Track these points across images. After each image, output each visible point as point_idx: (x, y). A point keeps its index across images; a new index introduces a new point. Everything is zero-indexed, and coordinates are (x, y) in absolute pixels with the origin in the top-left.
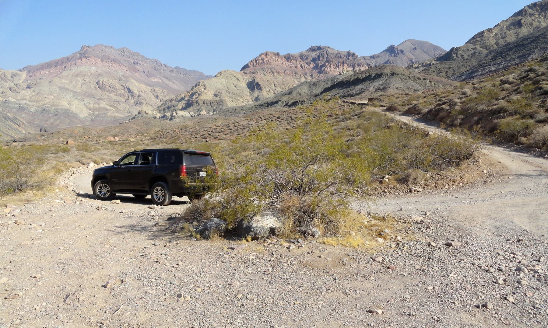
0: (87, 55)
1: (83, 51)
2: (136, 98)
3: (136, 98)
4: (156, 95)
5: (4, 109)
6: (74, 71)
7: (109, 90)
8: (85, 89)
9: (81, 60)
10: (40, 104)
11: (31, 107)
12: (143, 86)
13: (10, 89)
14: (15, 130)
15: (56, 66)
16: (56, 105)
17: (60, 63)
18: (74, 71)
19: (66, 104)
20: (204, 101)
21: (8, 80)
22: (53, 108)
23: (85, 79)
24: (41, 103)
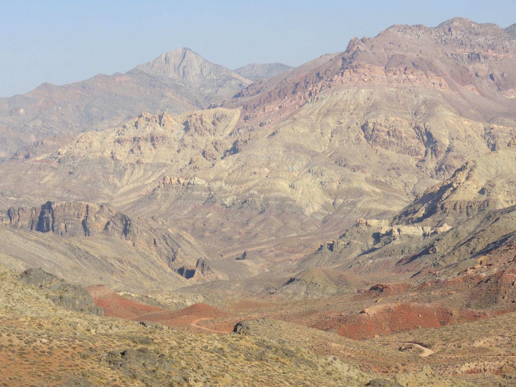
0: (354, 64)
1: (351, 53)
2: (441, 156)
3: (442, 155)
4: (493, 142)
5: (165, 221)
7: (385, 141)
10: (244, 187)
11: (227, 195)
12: (465, 123)
14: (158, 268)
15: (294, 92)
16: (268, 190)
17: (303, 84)
18: (324, 102)
19: (286, 186)
20: (456, 205)
21: (206, 129)
22: (262, 196)
23: (342, 121)
24: (243, 187)
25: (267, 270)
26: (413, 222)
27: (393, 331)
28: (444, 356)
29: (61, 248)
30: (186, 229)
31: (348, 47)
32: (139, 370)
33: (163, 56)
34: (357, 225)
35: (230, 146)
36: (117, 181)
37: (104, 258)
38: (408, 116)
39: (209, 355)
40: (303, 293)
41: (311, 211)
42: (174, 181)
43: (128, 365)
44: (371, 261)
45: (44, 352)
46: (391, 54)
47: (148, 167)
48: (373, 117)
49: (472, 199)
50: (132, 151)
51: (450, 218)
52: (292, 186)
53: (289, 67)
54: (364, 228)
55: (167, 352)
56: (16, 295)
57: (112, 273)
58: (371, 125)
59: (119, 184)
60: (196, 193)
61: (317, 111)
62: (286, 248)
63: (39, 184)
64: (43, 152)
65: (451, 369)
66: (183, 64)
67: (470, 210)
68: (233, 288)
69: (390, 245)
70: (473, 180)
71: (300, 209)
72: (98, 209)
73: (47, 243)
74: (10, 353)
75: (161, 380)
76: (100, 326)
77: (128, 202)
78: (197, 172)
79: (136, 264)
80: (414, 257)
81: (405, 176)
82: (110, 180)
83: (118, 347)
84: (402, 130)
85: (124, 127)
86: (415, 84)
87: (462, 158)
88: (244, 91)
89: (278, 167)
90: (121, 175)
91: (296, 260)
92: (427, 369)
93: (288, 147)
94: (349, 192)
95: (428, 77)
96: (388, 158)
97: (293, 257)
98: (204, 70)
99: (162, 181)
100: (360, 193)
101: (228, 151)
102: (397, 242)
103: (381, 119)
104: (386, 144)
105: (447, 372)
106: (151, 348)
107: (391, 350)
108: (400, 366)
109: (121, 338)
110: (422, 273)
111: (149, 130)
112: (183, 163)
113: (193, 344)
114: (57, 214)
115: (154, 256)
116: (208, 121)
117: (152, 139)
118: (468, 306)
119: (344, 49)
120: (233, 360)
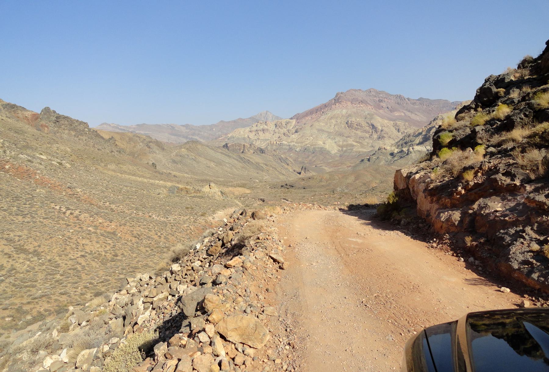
0: (340, 101)
1: (337, 97)
2: (379, 133)
6: (329, 115)
7: (356, 128)
8: (337, 129)
9: (335, 105)
10: (304, 144)
13: (284, 134)
14: (286, 169)
15: (316, 112)
17: (319, 109)
18: (329, 115)
19: (322, 143)
31: (336, 96)
41: (334, 152)
42: (275, 143)
46: (352, 98)
47: (262, 140)
48: (350, 119)
50: (256, 135)
57: (263, 171)
60: (284, 147)
61: (327, 118)
72: (249, 146)
73: (227, 154)
79: (274, 167)
84: (363, 123)
85: (252, 126)
86: (363, 108)
93: (319, 130)
94: (347, 146)
104: (356, 129)
111: (262, 127)
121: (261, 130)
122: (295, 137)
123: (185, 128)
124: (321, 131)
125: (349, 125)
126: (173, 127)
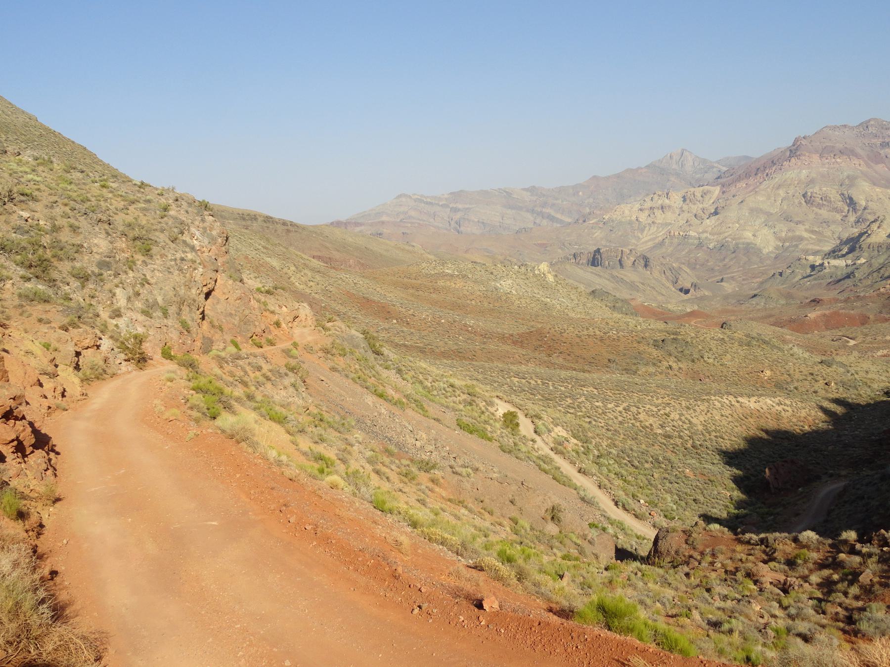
1: (796, 146)
2: (859, 213)
7: (819, 204)
10: (722, 236)
12: (878, 190)
15: (756, 174)
17: (762, 169)
18: (777, 180)
19: (751, 235)
20: (870, 245)
21: (697, 200)
23: (789, 192)
25: (737, 289)
26: (839, 257)
27: (827, 329)
28: (864, 345)
29: (606, 276)
30: (684, 264)
32: (673, 351)
33: (669, 155)
34: (799, 259)
35: (713, 211)
36: (639, 235)
37: (633, 282)
38: (836, 187)
39: (715, 342)
40: (763, 304)
41: (767, 251)
42: (676, 234)
43: (666, 348)
44: (809, 283)
45: (614, 339)
46: (824, 146)
49: (881, 241)
50: (649, 215)
51: (866, 254)
52: (754, 235)
53: (753, 158)
54: (804, 261)
55: (689, 340)
56: (589, 305)
57: (638, 291)
58: (809, 194)
59: (641, 236)
60: (690, 241)
61: (772, 186)
62: (750, 275)
63: (591, 238)
64: (594, 218)
65: (870, 354)
66: (682, 160)
67: (880, 248)
68: (715, 300)
69: (822, 273)
70: (883, 229)
71: (760, 250)
72: (628, 252)
74: (594, 340)
75: (687, 357)
76: (643, 324)
77: (647, 247)
78: (691, 228)
79: (652, 285)
80: (840, 280)
81: (833, 227)
82: (636, 234)
83: (659, 337)
84: (832, 196)
85: (644, 201)
87: (874, 213)
88: (722, 175)
89: (745, 223)
90: (642, 230)
91: (757, 282)
92: (855, 353)
93: (752, 210)
94: (793, 238)
95: (850, 160)
96: (821, 215)
97: (755, 280)
98: (695, 163)
99: (668, 234)
100: (801, 239)
101: (711, 214)
102: (826, 271)
103: (816, 189)
104: (820, 206)
105: (867, 356)
106: (679, 337)
107: (827, 341)
108: (834, 351)
109: (660, 331)
110: (846, 291)
111: (660, 202)
112: (682, 222)
113: (705, 336)
114: (604, 256)
115: (664, 280)
116: (698, 195)
117: (662, 208)
118: (881, 312)
119: (791, 144)
120: (731, 345)
121: (658, 208)
122: (710, 222)
123: (529, 194)
124: (755, 211)
125: (808, 199)
126: (508, 194)
